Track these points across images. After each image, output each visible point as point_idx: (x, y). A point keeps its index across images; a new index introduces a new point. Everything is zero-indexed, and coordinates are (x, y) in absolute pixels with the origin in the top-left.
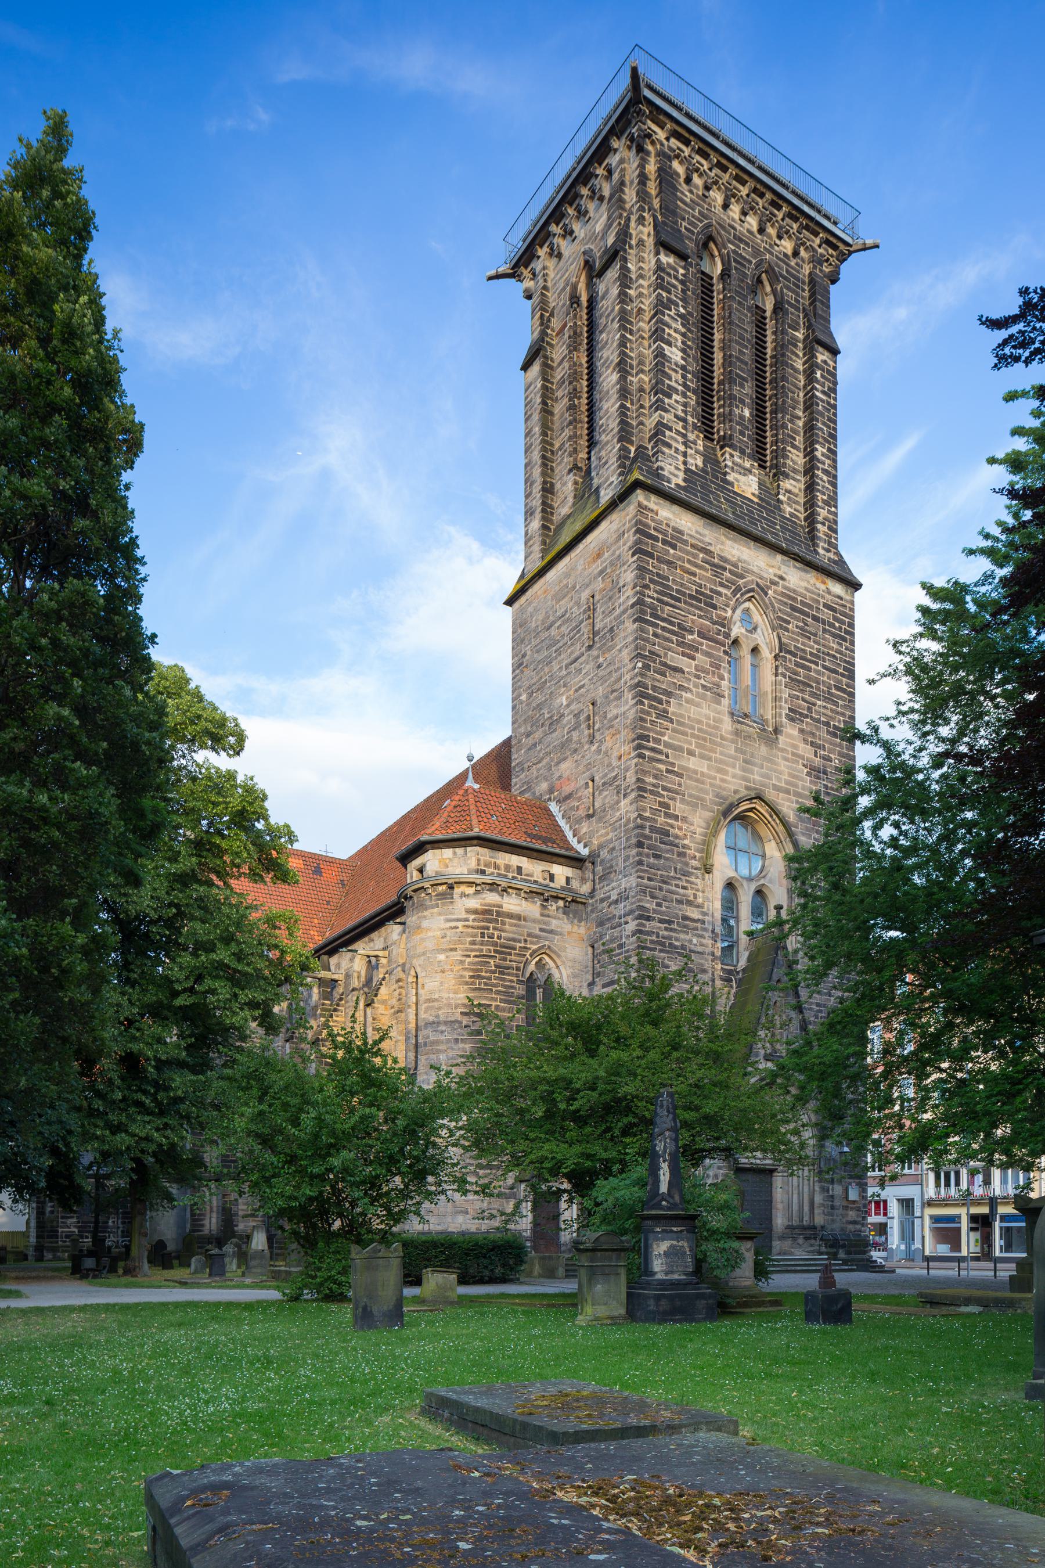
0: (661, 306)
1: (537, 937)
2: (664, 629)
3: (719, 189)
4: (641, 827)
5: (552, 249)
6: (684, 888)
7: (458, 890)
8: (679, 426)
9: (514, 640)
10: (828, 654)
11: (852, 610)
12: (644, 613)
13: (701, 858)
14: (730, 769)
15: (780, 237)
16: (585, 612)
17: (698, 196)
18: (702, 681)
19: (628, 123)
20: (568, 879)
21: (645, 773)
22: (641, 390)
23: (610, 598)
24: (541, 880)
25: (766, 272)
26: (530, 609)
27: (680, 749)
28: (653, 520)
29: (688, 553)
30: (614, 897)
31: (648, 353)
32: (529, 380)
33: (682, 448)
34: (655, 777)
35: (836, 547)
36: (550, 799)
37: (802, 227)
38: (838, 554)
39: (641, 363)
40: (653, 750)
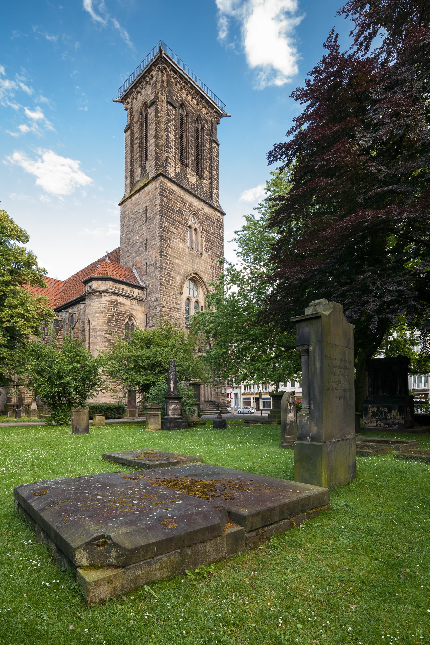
0: (168, 121)
8: (173, 158)
20: (139, 293)
21: (163, 263)
22: (162, 145)
27: (173, 257)
30: (153, 300)
31: (164, 135)
33: (174, 165)
34: (166, 264)
38: (219, 204)
39: (162, 137)
40: (165, 256)
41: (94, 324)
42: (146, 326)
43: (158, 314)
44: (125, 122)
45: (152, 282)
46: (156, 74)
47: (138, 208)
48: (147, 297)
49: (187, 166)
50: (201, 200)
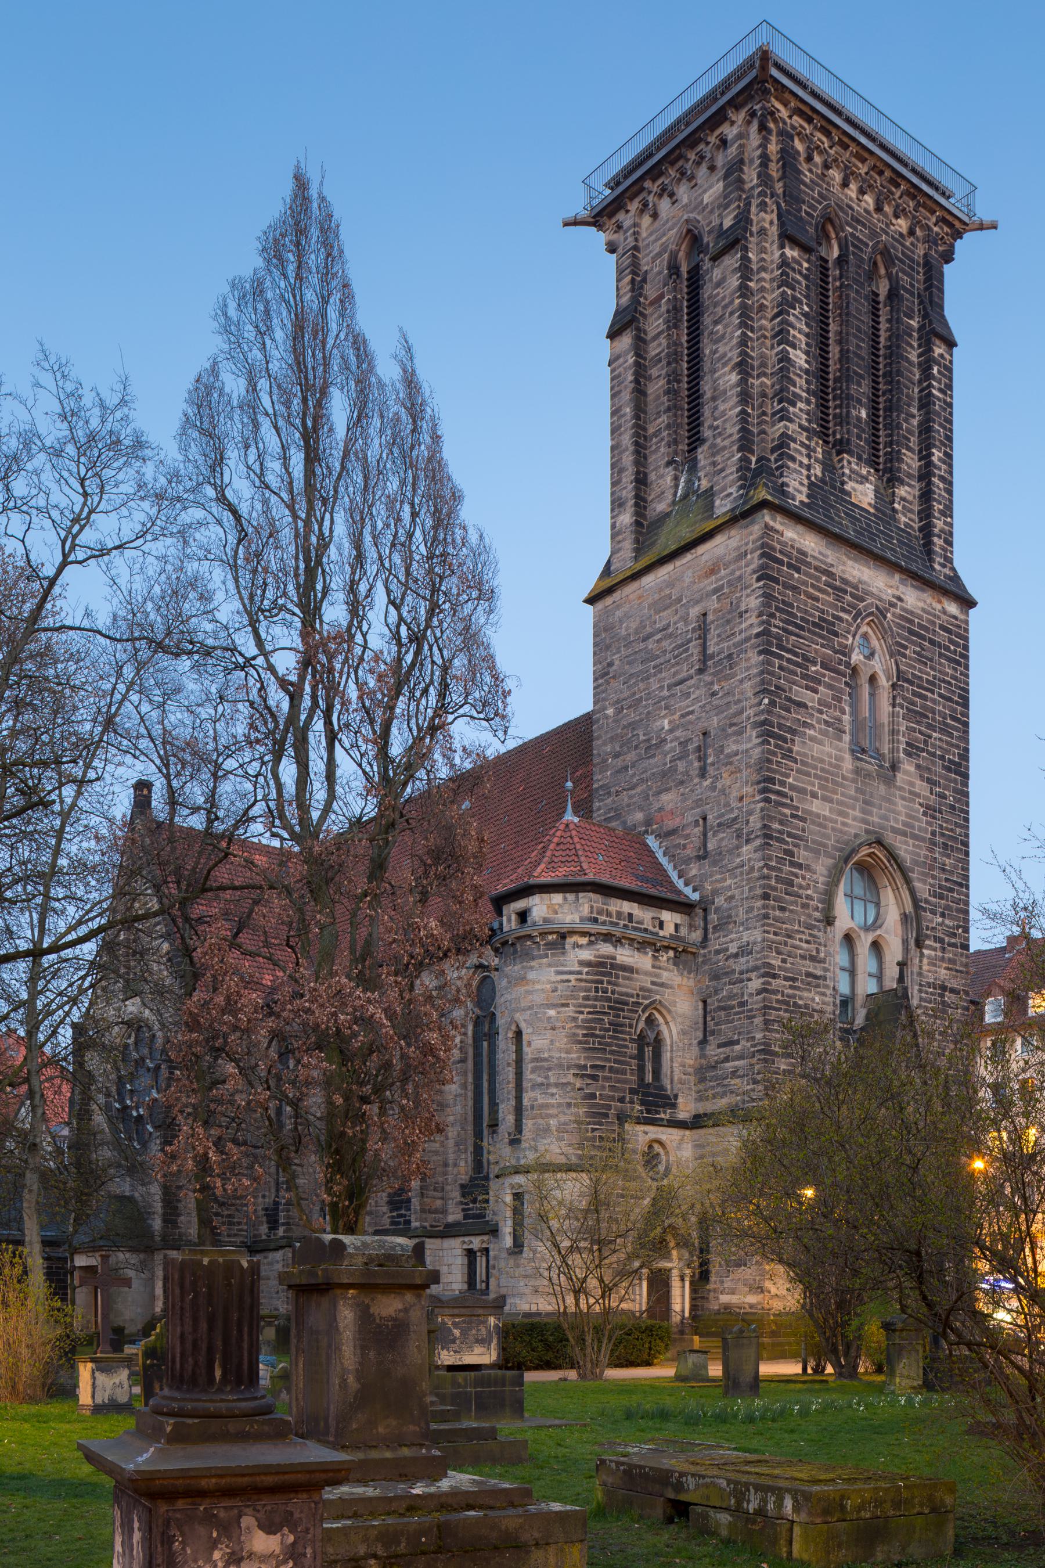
0: (785, 305)
1: (649, 991)
2: (789, 661)
3: (838, 167)
6: (808, 942)
7: (570, 940)
9: (595, 645)
10: (944, 681)
11: (967, 630)
12: (770, 644)
13: (823, 909)
15: (897, 217)
16: (694, 630)
17: (817, 175)
18: (825, 717)
19: (751, 97)
20: (677, 926)
21: (771, 818)
22: (764, 395)
23: (728, 622)
24: (650, 928)
25: (881, 253)
26: (619, 613)
27: (802, 791)
28: (779, 542)
29: (811, 576)
30: (733, 949)
31: (772, 354)
32: (617, 351)
33: (805, 461)
34: (781, 823)
36: (646, 832)
37: (918, 204)
38: (953, 569)
39: (763, 365)
41: (536, 1043)
42: (703, 1042)
43: (756, 1002)
45: (732, 886)
46: (740, 136)
47: (666, 617)
48: (705, 938)
49: (841, 447)
50: (893, 566)
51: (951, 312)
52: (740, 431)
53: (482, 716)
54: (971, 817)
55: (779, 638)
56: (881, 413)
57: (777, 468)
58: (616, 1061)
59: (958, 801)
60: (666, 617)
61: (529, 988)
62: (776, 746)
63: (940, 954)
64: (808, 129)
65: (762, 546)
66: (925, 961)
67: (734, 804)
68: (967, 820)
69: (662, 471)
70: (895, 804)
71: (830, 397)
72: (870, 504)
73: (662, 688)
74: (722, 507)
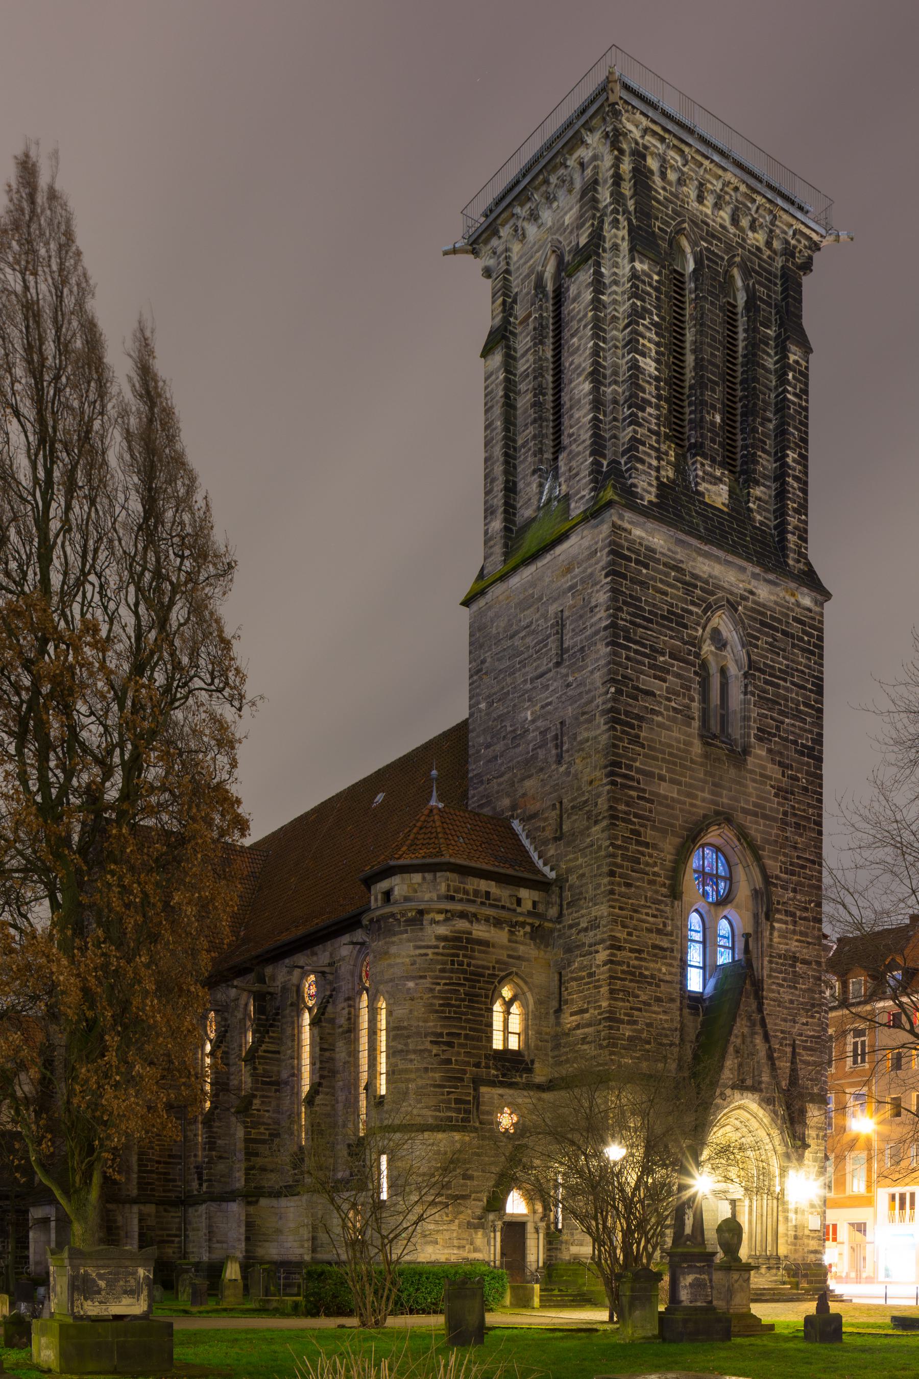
0: (636, 315)
1: (505, 963)
2: (636, 652)
4: (613, 856)
5: (516, 231)
6: (654, 916)
7: (427, 917)
9: (471, 644)
10: (797, 670)
11: (821, 622)
12: (618, 637)
13: (670, 885)
14: (699, 793)
16: (552, 626)
18: (673, 704)
20: (535, 904)
22: (615, 402)
23: (581, 617)
24: (508, 905)
26: (491, 614)
27: (650, 775)
28: (626, 539)
30: (584, 925)
32: (490, 369)
33: (655, 463)
34: (627, 804)
35: (805, 557)
36: (512, 816)
38: (808, 564)
39: (616, 373)
40: (625, 776)
44: (483, 317)
47: (528, 616)
48: (561, 915)
51: (808, 322)
52: (591, 436)
53: (213, 687)
54: (824, 798)
55: (625, 630)
56: (739, 418)
57: (627, 471)
58: (471, 1029)
59: (812, 783)
60: (528, 616)
61: (391, 961)
62: (623, 732)
63: (791, 927)
64: (661, 148)
65: (610, 544)
66: (776, 934)
67: (586, 788)
68: (820, 801)
69: (529, 479)
70: (746, 786)
71: (686, 403)
72: (723, 504)
73: (525, 681)
74: (577, 509)
